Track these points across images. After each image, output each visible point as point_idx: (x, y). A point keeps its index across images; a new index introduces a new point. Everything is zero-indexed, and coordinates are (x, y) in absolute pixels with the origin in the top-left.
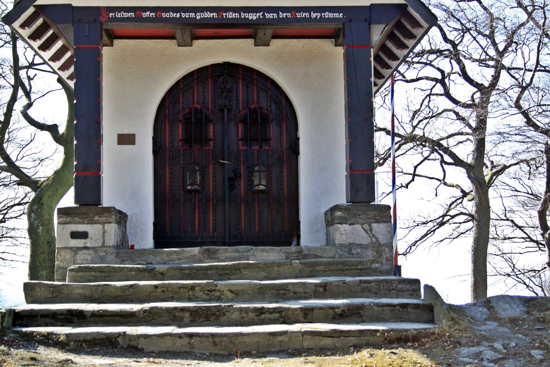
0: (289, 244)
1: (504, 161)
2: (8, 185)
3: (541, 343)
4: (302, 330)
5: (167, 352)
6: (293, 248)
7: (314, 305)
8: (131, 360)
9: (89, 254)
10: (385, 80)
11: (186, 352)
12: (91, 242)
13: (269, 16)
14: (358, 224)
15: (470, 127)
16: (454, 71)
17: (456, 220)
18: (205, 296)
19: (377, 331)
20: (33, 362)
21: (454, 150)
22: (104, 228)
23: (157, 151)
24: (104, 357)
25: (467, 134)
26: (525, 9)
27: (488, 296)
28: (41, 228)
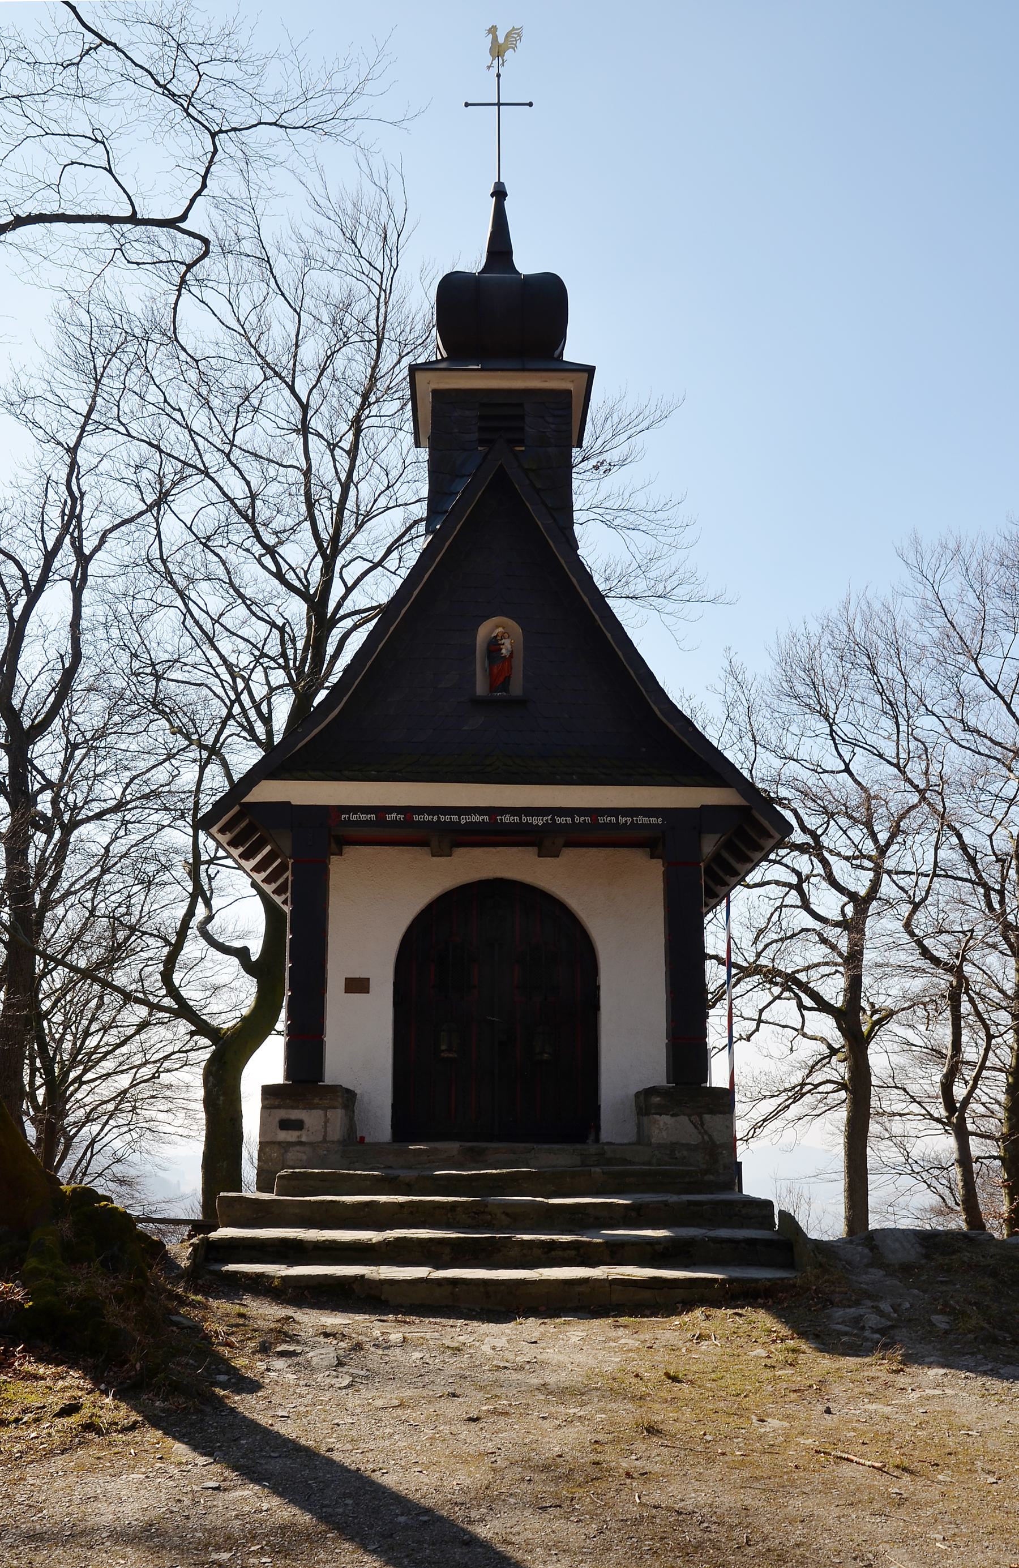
0: (582, 1139)
1: (889, 1003)
2: (166, 1023)
3: (946, 1305)
4: (610, 1278)
6: (592, 1148)
7: (625, 1238)
8: (374, 1318)
9: (304, 1153)
10: (718, 899)
11: (447, 1306)
12: (307, 1135)
13: (559, 820)
14: (684, 1115)
15: (840, 955)
16: (814, 873)
17: (821, 1089)
20: (241, 1321)
22: (326, 1115)
24: (334, 1313)
25: (836, 964)
27: (870, 1227)
28: (221, 1098)
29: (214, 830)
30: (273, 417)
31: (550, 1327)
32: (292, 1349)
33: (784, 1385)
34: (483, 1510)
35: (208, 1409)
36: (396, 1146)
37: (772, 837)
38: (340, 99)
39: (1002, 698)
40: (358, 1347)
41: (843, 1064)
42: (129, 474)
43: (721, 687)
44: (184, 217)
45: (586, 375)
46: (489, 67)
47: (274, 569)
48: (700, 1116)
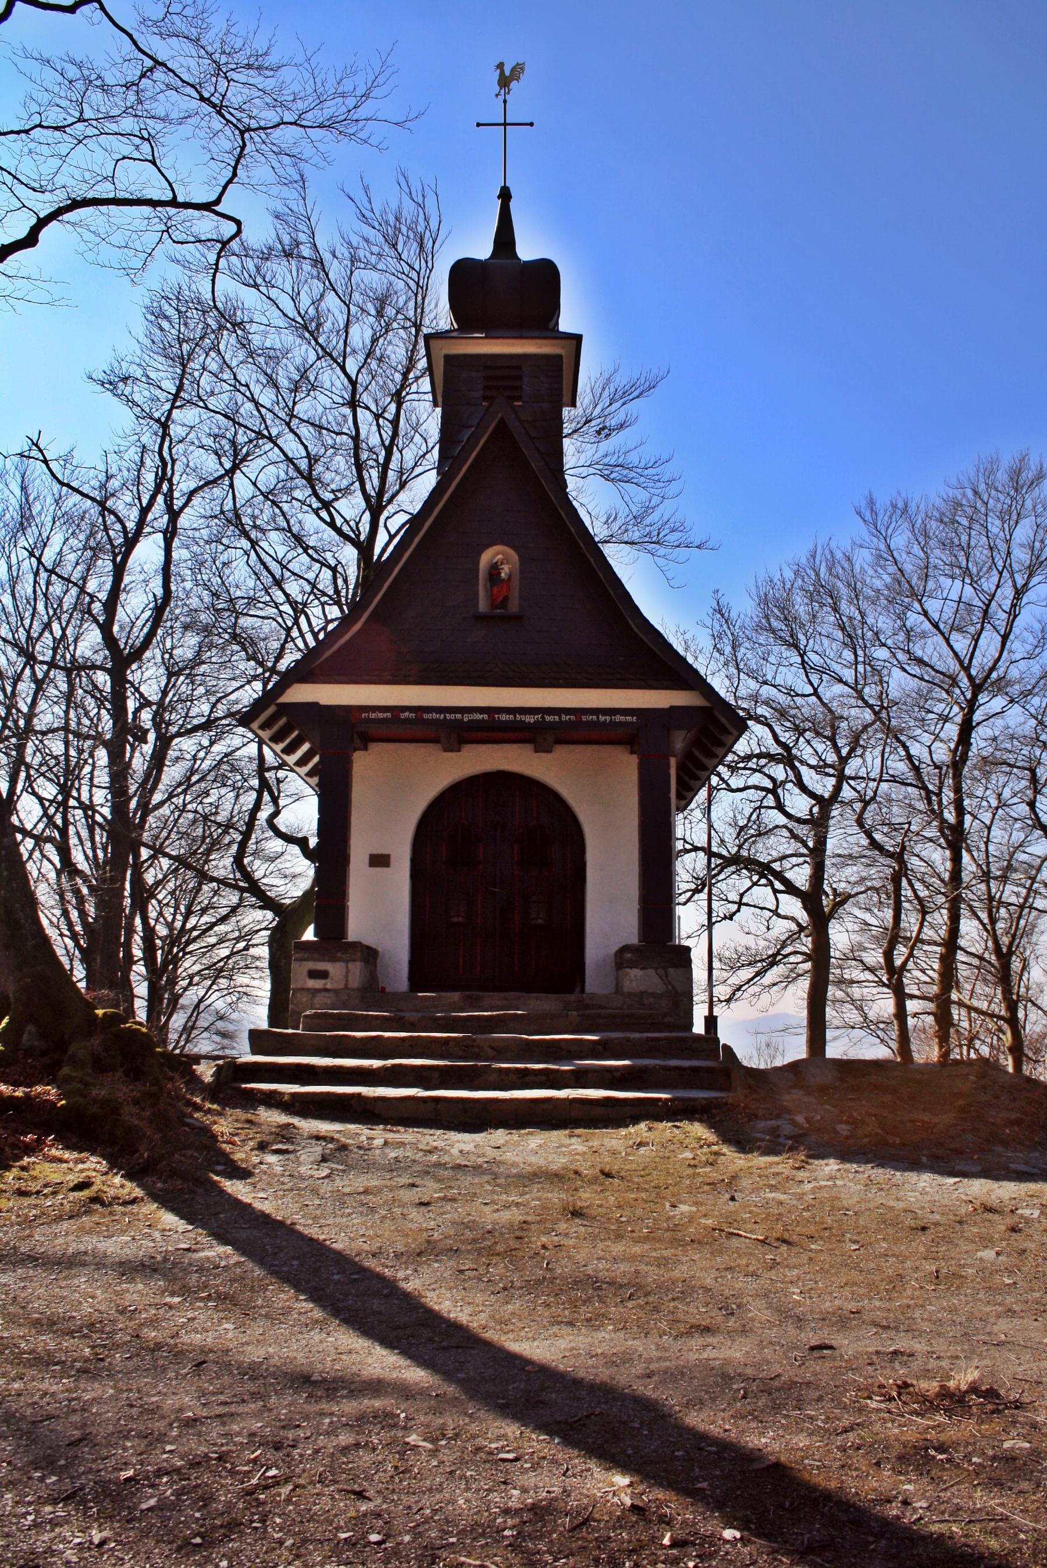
0: (571, 991)
5: (408, 1119)
6: (572, 997)
13: (548, 718)
15: (806, 846)
18: (461, 1053)
19: (660, 1099)
21: (788, 875)
23: (414, 876)
26: (871, 707)
29: (255, 725)
30: (329, 394)
31: (515, 1136)
32: (285, 1147)
33: (701, 1179)
34: (409, 1272)
35: (200, 1191)
36: (412, 994)
37: (731, 734)
38: (351, 102)
39: (942, 634)
40: (344, 1147)
41: (810, 939)
42: (209, 442)
43: (709, 623)
44: (218, 201)
45: (574, 342)
46: (497, 95)
47: (328, 519)
48: (665, 969)
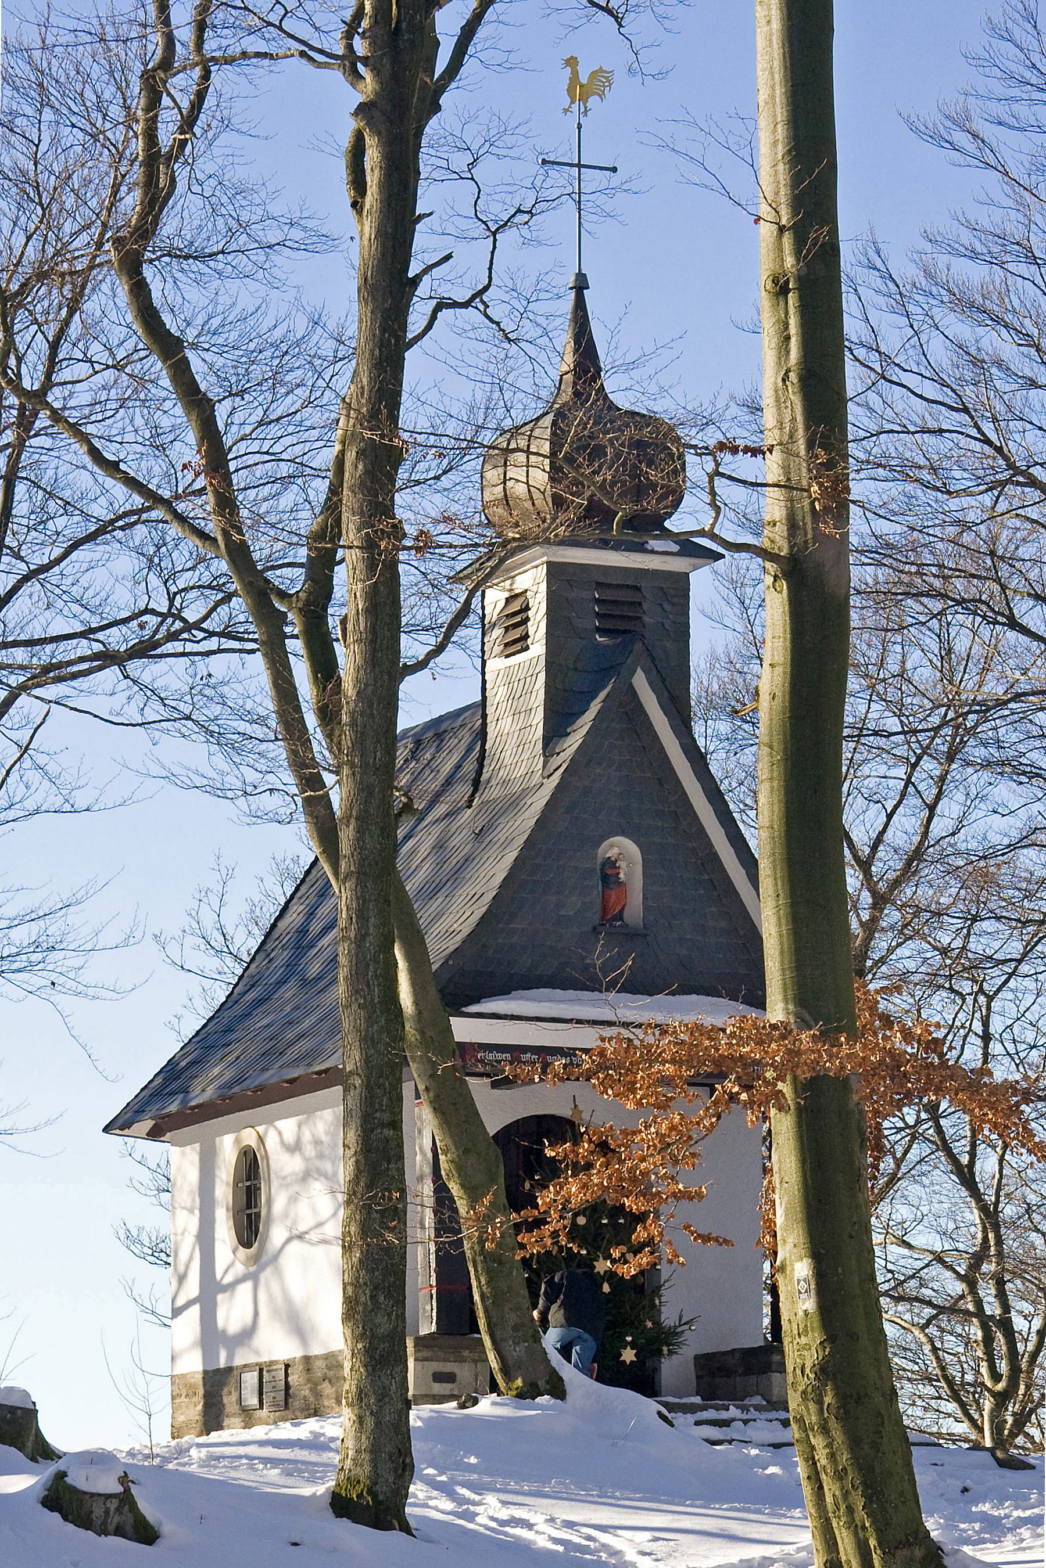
46: (566, 111)
